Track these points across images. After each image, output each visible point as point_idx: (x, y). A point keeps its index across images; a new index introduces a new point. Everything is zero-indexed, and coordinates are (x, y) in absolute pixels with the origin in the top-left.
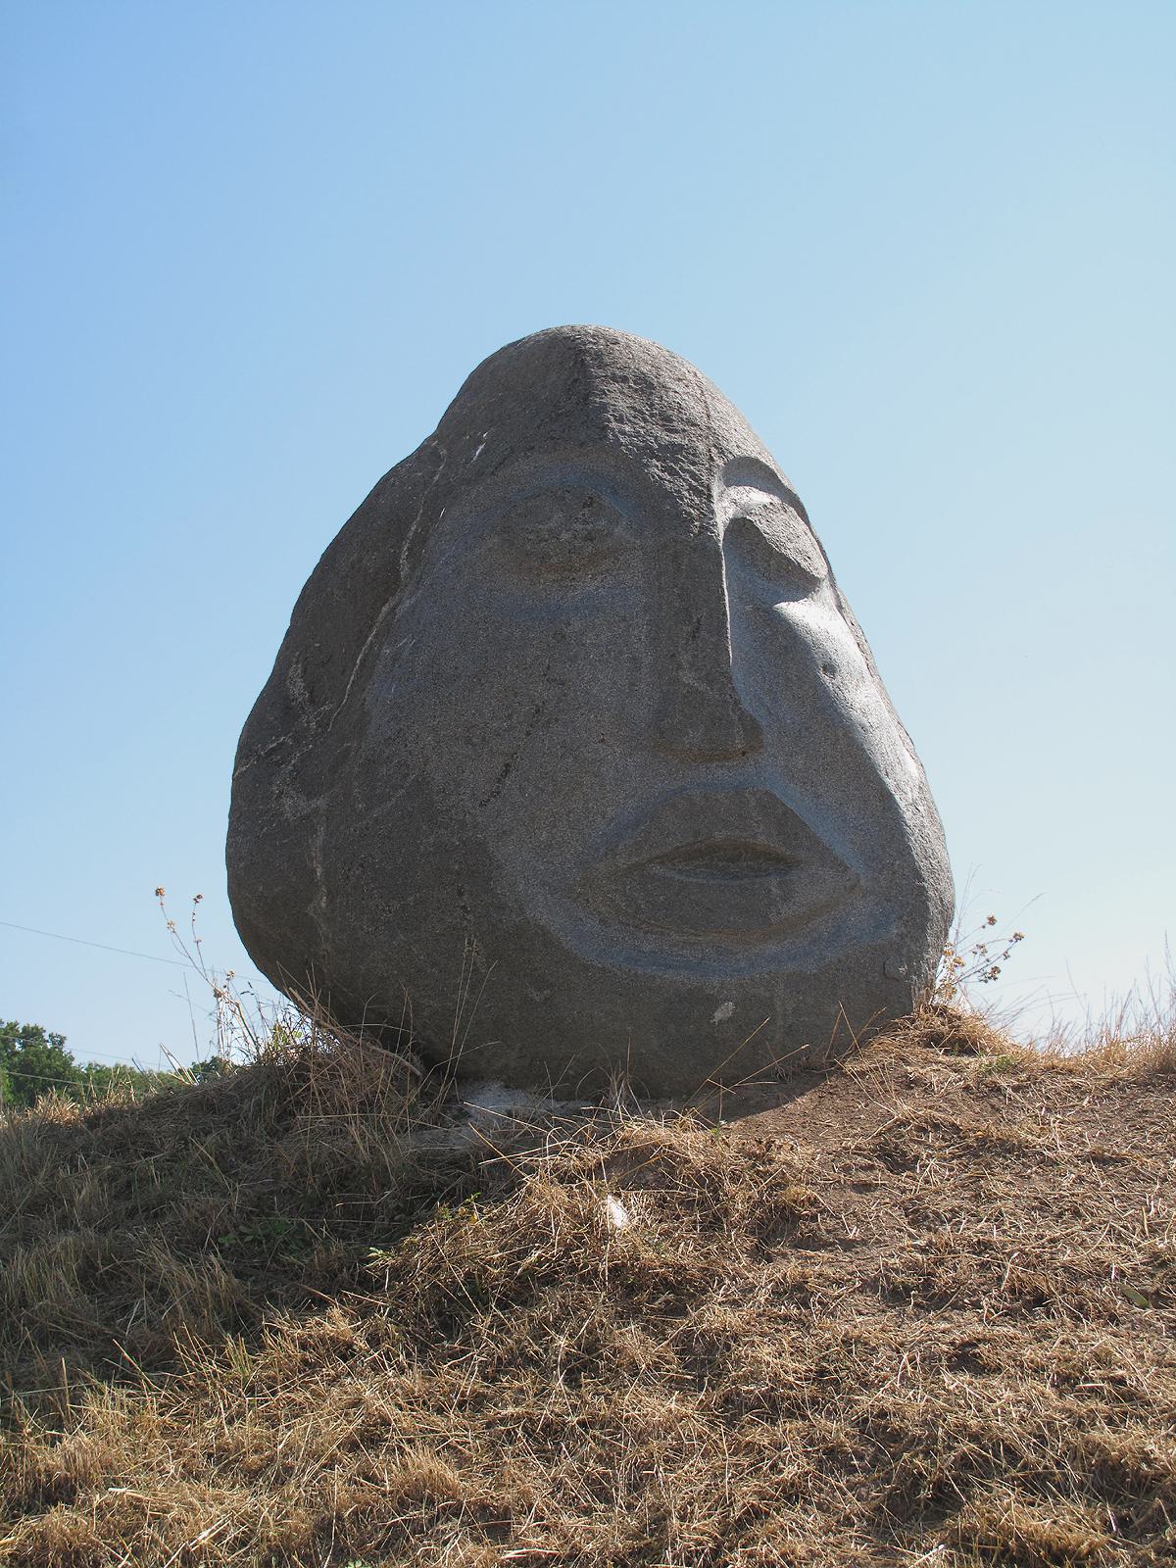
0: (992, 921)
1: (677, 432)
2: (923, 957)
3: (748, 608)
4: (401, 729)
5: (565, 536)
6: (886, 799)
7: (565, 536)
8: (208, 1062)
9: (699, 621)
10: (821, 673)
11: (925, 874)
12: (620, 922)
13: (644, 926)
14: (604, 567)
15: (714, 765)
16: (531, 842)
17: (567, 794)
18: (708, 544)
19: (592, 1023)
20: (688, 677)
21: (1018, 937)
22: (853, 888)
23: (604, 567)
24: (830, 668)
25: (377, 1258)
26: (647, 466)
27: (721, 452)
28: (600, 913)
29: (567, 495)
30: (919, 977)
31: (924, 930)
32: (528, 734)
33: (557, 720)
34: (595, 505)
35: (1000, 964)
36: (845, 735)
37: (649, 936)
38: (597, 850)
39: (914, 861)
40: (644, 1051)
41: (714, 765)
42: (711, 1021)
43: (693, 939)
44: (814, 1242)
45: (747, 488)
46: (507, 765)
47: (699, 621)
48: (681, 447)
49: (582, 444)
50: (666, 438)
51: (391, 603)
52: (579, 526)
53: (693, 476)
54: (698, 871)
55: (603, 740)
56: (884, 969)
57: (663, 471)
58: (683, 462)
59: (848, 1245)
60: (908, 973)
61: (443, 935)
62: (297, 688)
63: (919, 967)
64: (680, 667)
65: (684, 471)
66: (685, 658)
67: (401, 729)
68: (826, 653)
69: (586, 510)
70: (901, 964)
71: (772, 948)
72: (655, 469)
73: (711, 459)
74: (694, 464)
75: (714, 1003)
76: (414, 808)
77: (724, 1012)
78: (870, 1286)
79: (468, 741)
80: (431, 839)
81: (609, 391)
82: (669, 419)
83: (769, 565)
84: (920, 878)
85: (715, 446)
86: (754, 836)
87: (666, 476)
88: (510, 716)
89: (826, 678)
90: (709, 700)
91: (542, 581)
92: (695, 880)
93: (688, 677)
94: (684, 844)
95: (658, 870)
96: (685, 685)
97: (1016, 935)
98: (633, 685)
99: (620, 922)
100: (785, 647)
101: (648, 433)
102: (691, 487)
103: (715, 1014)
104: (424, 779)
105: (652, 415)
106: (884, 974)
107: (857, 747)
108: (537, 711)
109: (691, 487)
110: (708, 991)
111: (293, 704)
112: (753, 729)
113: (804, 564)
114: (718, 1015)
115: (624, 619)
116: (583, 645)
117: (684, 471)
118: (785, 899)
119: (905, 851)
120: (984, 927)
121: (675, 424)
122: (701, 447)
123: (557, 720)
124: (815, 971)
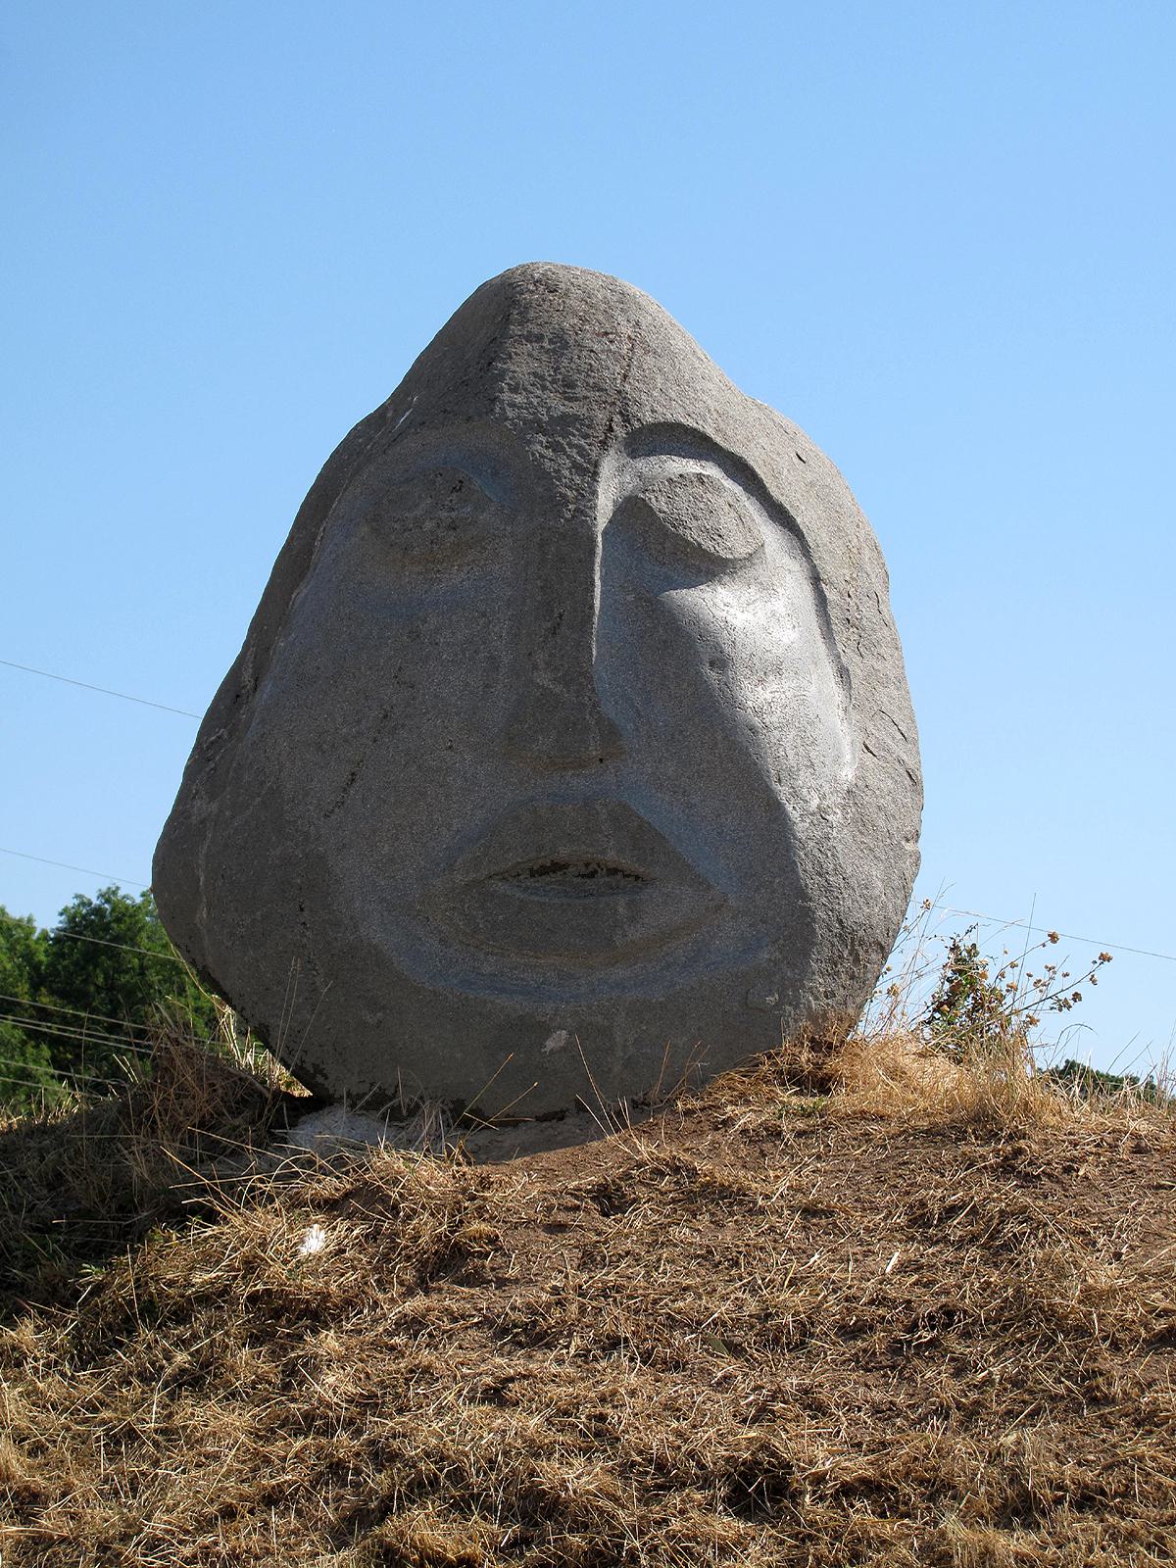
0: (1053, 938)
1: (577, 399)
2: (803, 986)
3: (631, 598)
4: (264, 733)
5: (428, 525)
6: (775, 808)
7: (428, 525)
8: (1061, 1068)
9: (561, 616)
10: (706, 669)
11: (814, 892)
12: (461, 942)
13: (484, 947)
14: (470, 558)
15: (570, 773)
16: (372, 856)
17: (409, 805)
18: (580, 530)
19: (422, 1048)
20: (543, 679)
21: (1105, 958)
22: (718, 908)
23: (470, 558)
24: (721, 662)
25: (88, 1274)
26: (529, 442)
27: (626, 420)
28: (441, 932)
29: (439, 478)
30: (796, 1007)
31: (807, 955)
32: (375, 741)
33: (403, 726)
34: (463, 490)
35: (1084, 989)
36: (725, 738)
37: (490, 957)
38: (438, 864)
39: (798, 878)
40: (472, 1080)
41: (570, 773)
42: (543, 1050)
43: (533, 961)
44: (475, 1280)
45: (664, 457)
46: (353, 774)
47: (561, 616)
48: (576, 418)
49: (469, 419)
50: (561, 407)
51: (297, 591)
52: (444, 514)
53: (581, 451)
54: (548, 888)
55: (450, 747)
56: (747, 998)
57: (547, 448)
58: (574, 436)
59: (502, 1283)
60: (778, 1005)
61: (286, 952)
62: (247, 677)
63: (797, 997)
64: (535, 667)
65: (571, 445)
66: (540, 657)
67: (264, 733)
68: (718, 648)
69: (454, 495)
70: (771, 994)
71: (620, 973)
72: (539, 446)
73: (611, 429)
74: (586, 436)
75: (546, 1031)
76: (266, 817)
77: (556, 1041)
78: (487, 1322)
79: (319, 747)
80: (278, 851)
81: (516, 354)
82: (571, 385)
83: (664, 548)
84: (806, 898)
85: (621, 413)
86: (603, 852)
87: (549, 453)
88: (359, 722)
89: (712, 675)
90: (564, 702)
91: (407, 574)
92: (536, 899)
93: (543, 679)
94: (525, 860)
95: (501, 887)
96: (539, 687)
97: (1102, 954)
98: (487, 686)
99: (461, 942)
100: (665, 642)
101: (542, 403)
102: (576, 466)
103: (547, 1043)
104: (278, 787)
105: (553, 382)
106: (746, 1004)
107: (741, 750)
108: (385, 717)
109: (576, 466)
110: (538, 1018)
111: (243, 691)
112: (611, 733)
113: (708, 545)
114: (550, 1044)
115: (484, 615)
116: (437, 644)
117: (571, 445)
118: (633, 920)
119: (789, 867)
120: (1044, 945)
121: (578, 390)
122: (601, 416)
123: (403, 726)
124: (662, 999)
